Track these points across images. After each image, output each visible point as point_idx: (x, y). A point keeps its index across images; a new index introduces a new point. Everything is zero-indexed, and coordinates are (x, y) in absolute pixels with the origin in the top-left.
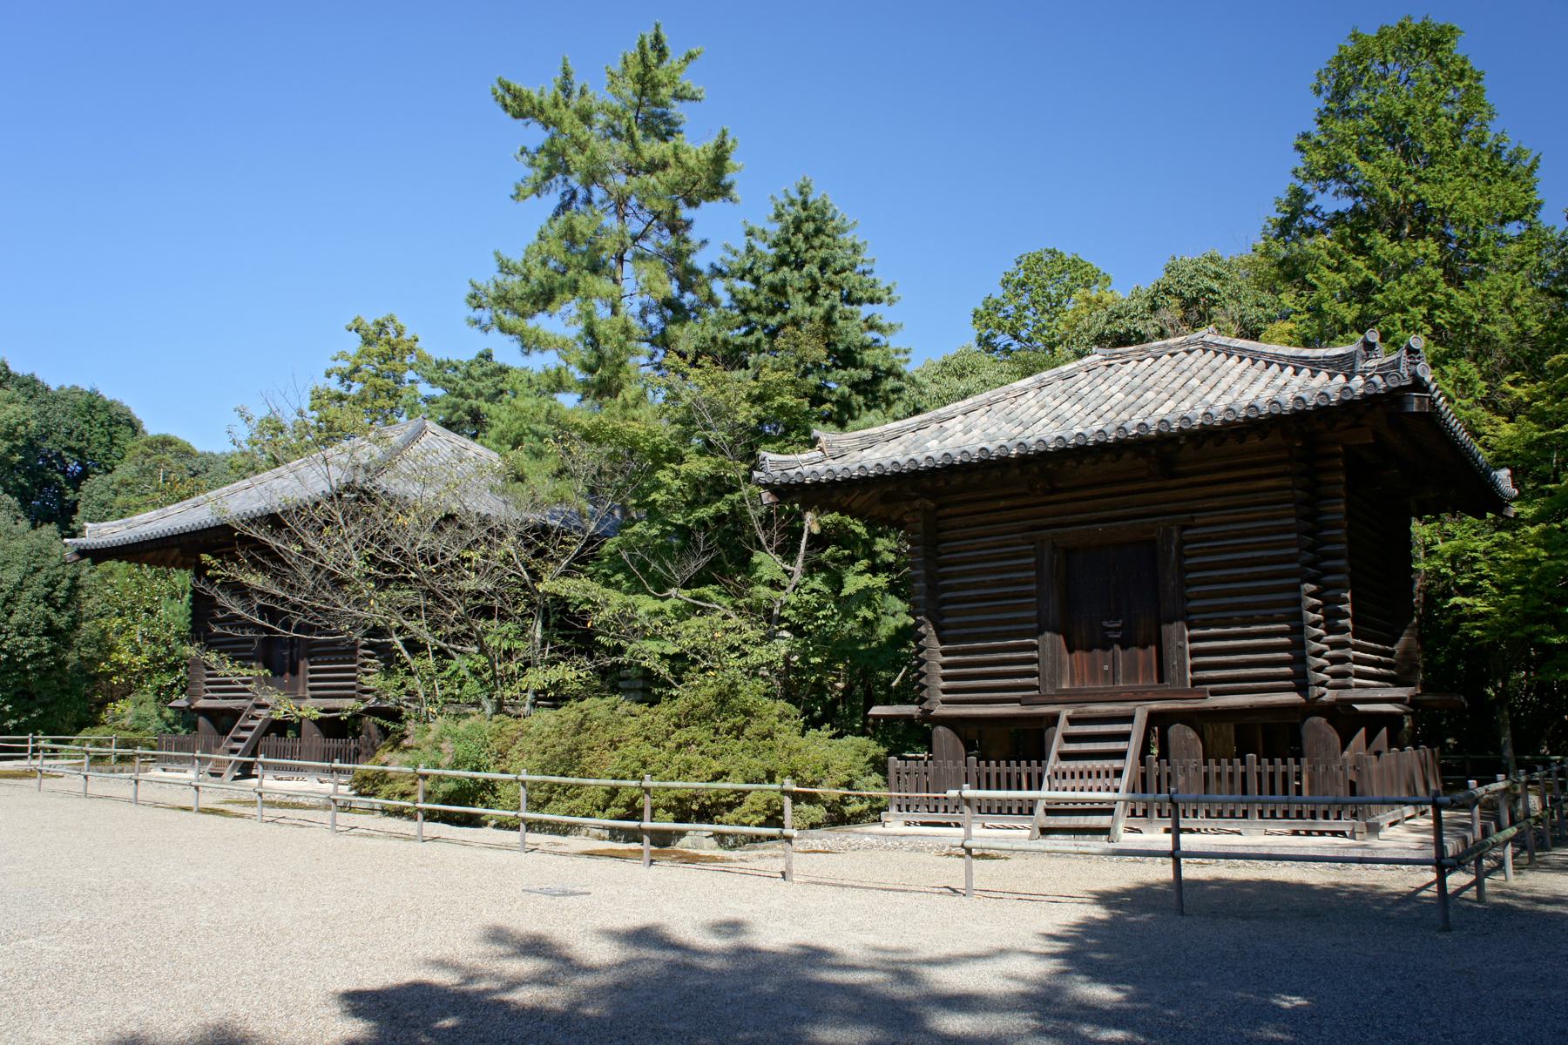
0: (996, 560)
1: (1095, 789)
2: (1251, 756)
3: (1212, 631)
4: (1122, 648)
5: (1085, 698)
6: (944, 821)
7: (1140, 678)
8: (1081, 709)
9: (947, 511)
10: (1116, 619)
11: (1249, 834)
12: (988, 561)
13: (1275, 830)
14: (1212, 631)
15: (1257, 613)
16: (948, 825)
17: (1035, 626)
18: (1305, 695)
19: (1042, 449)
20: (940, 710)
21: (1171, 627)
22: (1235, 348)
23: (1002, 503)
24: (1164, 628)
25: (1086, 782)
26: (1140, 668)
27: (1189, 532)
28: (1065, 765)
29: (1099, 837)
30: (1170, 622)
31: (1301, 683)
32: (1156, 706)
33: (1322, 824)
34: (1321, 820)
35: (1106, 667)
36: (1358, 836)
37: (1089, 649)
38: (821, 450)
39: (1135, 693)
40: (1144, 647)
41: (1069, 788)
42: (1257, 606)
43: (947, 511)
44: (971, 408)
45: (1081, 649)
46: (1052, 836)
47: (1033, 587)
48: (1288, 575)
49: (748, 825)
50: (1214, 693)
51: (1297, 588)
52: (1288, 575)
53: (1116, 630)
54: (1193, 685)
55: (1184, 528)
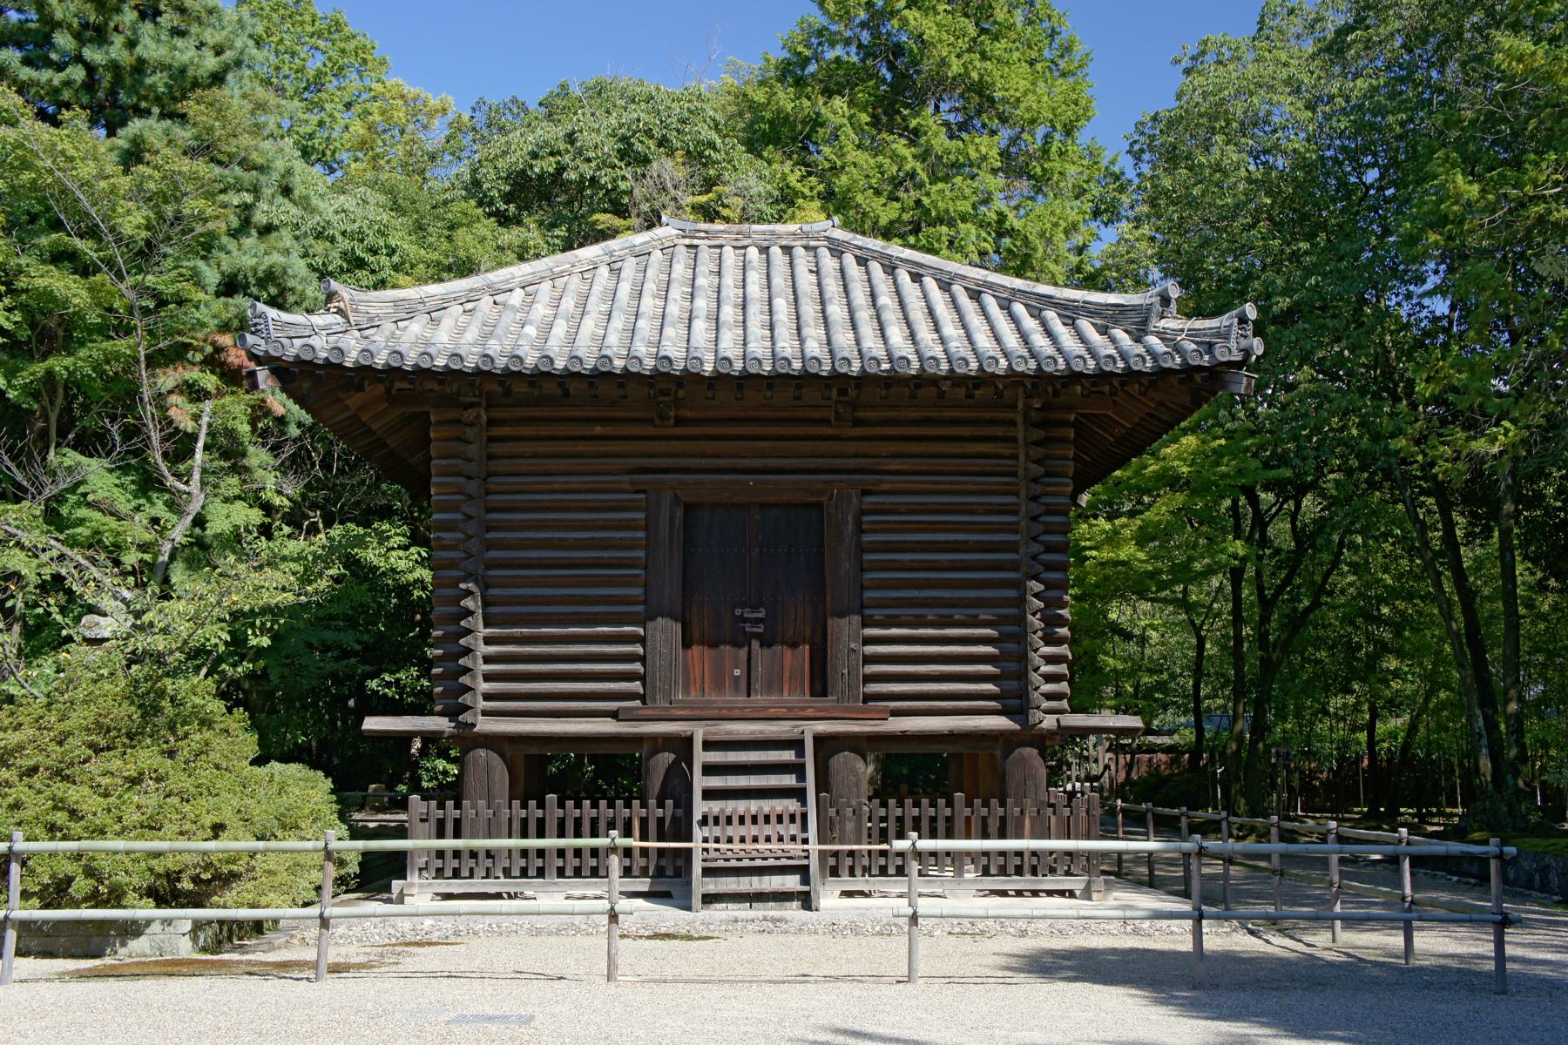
0: (962, 512)
1: (761, 839)
2: (552, 798)
3: (895, 631)
4: (762, 646)
5: (716, 713)
6: (492, 890)
7: (786, 688)
8: (713, 729)
9: (506, 431)
10: (755, 608)
11: (956, 896)
12: (568, 510)
13: (590, 892)
14: (895, 631)
15: (931, 614)
16: (498, 896)
17: (640, 608)
18: (1024, 722)
19: (307, 357)
20: (485, 725)
21: (844, 622)
22: (902, 260)
23: (598, 430)
24: (832, 623)
25: (761, 830)
26: (787, 675)
27: (869, 499)
28: (715, 807)
29: (787, 904)
30: (842, 615)
31: (1015, 702)
32: (822, 727)
33: (477, 885)
34: (1028, 877)
35: (737, 672)
36: (1095, 895)
37: (714, 645)
38: (340, 312)
39: (790, 709)
40: (794, 645)
41: (736, 839)
42: (954, 604)
43: (506, 431)
44: (530, 279)
45: (702, 643)
46: (718, 906)
47: (641, 554)
48: (1014, 566)
49: (267, 906)
50: (897, 713)
51: (1019, 585)
52: (1014, 566)
53: (757, 621)
54: (865, 701)
55: (865, 493)
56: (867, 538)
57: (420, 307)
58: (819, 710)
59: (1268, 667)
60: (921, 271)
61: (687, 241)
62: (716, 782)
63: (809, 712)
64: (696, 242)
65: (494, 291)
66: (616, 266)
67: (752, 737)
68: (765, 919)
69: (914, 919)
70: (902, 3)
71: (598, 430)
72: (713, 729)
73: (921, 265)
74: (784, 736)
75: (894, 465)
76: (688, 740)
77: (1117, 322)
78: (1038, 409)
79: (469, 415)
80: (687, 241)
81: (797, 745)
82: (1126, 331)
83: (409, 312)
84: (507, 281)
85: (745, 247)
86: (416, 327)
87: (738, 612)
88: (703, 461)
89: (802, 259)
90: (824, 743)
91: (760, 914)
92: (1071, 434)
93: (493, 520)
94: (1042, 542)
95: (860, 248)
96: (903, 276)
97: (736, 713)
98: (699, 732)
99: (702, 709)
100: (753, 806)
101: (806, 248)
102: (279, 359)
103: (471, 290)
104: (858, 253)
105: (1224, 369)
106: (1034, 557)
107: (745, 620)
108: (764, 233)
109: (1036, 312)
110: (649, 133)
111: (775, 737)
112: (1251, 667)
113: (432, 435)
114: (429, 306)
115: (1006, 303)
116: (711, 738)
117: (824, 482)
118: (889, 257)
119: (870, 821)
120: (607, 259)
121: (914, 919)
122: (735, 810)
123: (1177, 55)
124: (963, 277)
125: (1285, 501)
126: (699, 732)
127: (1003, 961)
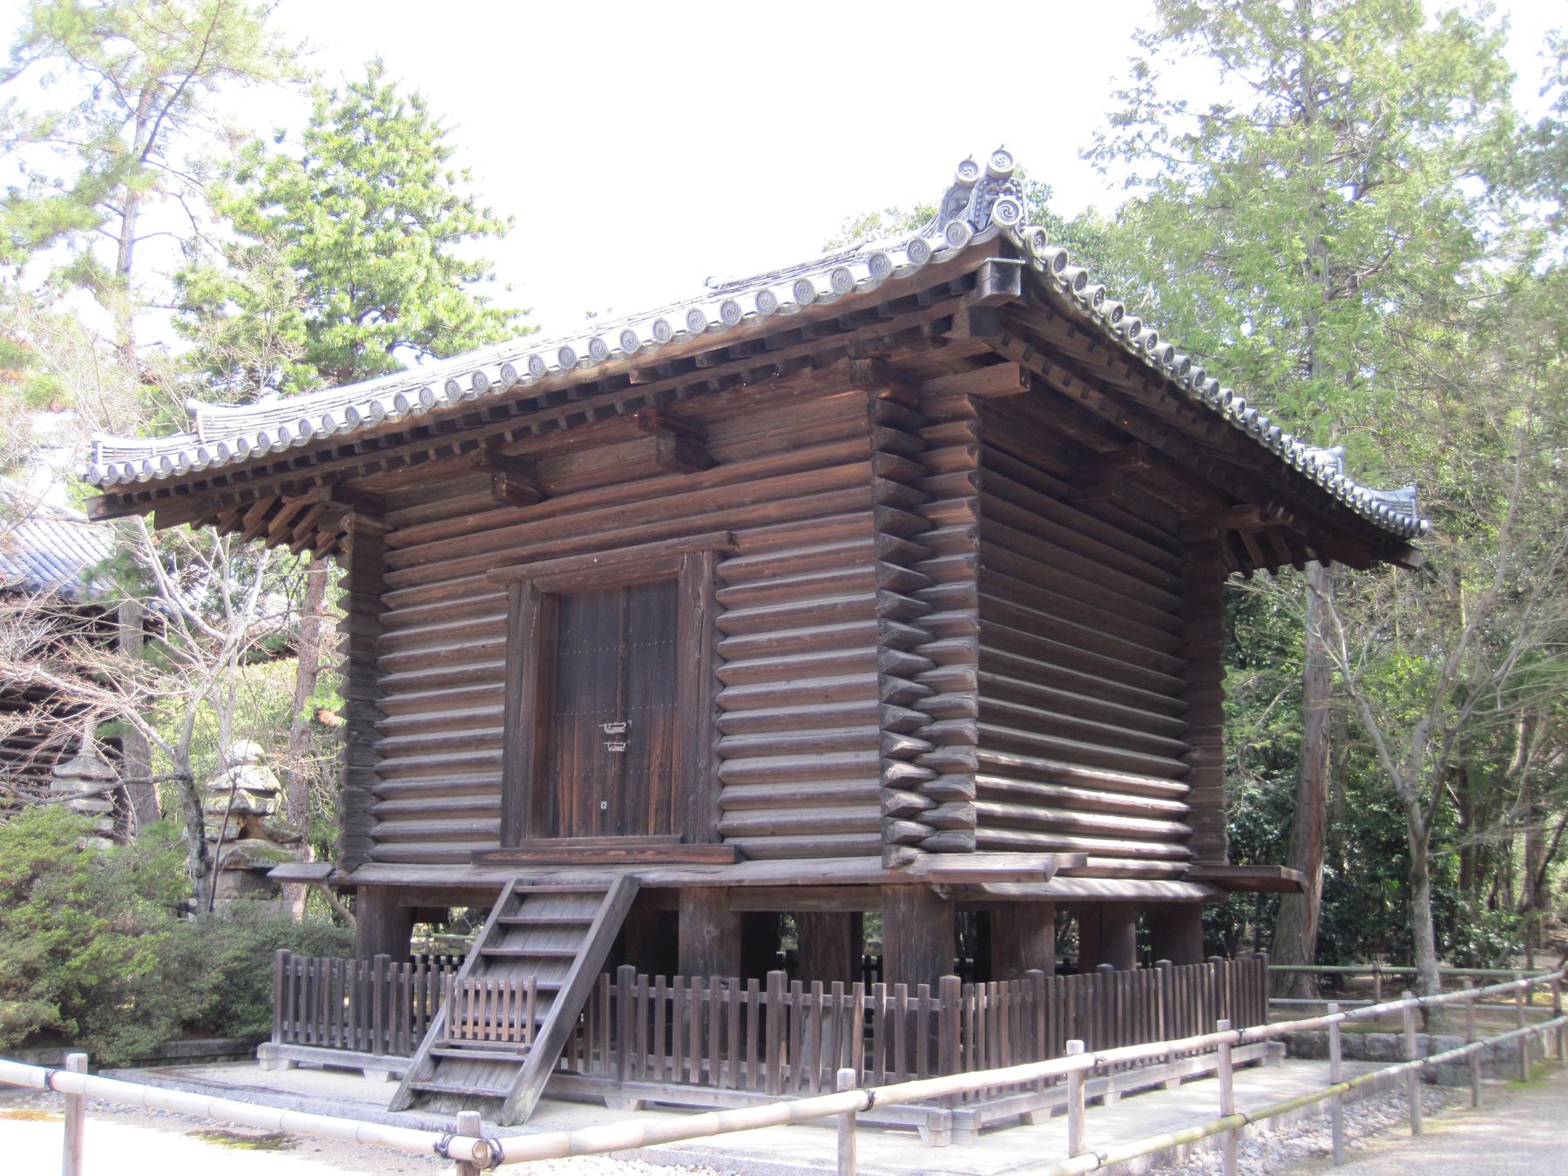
7: (652, 824)
8: (546, 878)
63: (649, 855)
97: (575, 858)
99: (544, 852)
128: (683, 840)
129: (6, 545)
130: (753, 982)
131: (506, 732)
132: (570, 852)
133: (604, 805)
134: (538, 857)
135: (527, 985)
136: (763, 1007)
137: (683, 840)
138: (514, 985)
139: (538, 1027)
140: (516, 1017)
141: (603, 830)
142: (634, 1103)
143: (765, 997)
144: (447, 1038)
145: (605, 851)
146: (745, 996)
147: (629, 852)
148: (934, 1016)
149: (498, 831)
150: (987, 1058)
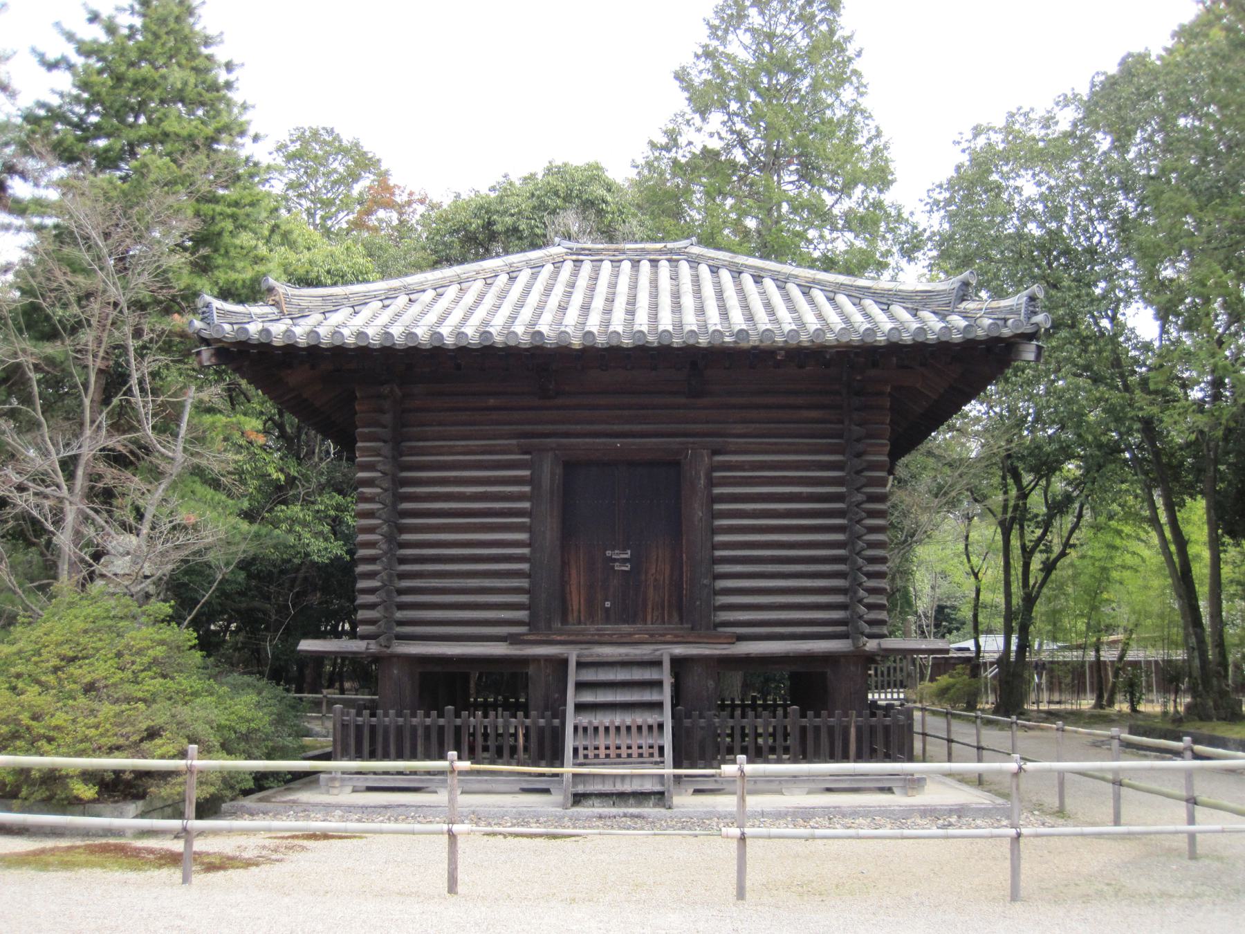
7: (649, 618)
8: (586, 652)
22: (746, 266)
23: (492, 402)
32: (679, 650)
38: (276, 304)
53: (624, 561)
55: (716, 452)
56: (717, 491)
57: (345, 301)
58: (676, 636)
59: (1029, 600)
60: (762, 274)
61: (574, 257)
62: (588, 697)
63: (669, 638)
64: (581, 257)
65: (410, 291)
66: (514, 275)
67: (619, 659)
68: (625, 815)
69: (743, 838)
70: (748, 3)
71: (492, 402)
72: (586, 652)
73: (762, 269)
74: (646, 658)
75: (739, 429)
76: (564, 662)
77: (925, 306)
78: (775, 741)
79: (386, 389)
80: (574, 257)
81: (657, 664)
82: (934, 313)
83: (335, 305)
84: (421, 283)
85: (621, 261)
86: (335, 318)
87: (608, 553)
88: (579, 427)
89: (664, 267)
90: (679, 664)
91: (621, 810)
92: (888, 403)
93: (406, 477)
94: (864, 541)
95: (713, 259)
96: (747, 279)
97: (606, 638)
98: (573, 654)
99: (577, 635)
100: (618, 719)
101: (669, 260)
102: (219, 340)
103: (390, 290)
104: (711, 262)
105: (1018, 340)
106: (858, 505)
107: (615, 560)
108: (636, 250)
109: (857, 301)
110: (556, 194)
111: (638, 659)
112: (1016, 601)
113: (357, 408)
114: (352, 302)
115: (831, 295)
116: (583, 660)
117: (680, 443)
118: (736, 264)
119: (607, 610)
120: (507, 269)
121: (743, 838)
122: (645, 721)
123: (958, 138)
124: (796, 277)
125: (1040, 479)
126: (573, 654)
127: (96, 34)
128: (692, 629)
129: (1242, 274)
130: (434, 713)
131: (531, 538)
132: (600, 635)
133: (608, 604)
134: (572, 638)
135: (645, 721)
136: (743, 728)
137: (692, 629)
138: (596, 723)
139: (661, 749)
140: (642, 742)
141: (607, 620)
142: (350, 788)
143: (442, 721)
144: (657, 758)
145: (630, 635)
146: (428, 721)
147: (652, 636)
148: (871, 727)
149: (527, 620)
150: (887, 744)
